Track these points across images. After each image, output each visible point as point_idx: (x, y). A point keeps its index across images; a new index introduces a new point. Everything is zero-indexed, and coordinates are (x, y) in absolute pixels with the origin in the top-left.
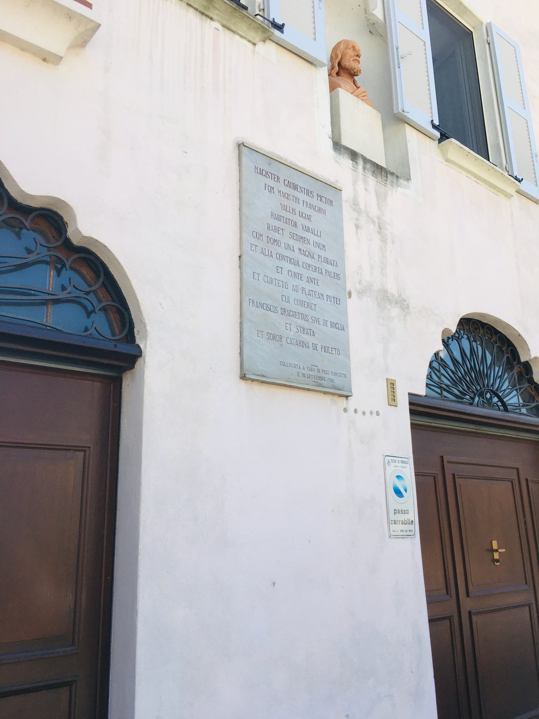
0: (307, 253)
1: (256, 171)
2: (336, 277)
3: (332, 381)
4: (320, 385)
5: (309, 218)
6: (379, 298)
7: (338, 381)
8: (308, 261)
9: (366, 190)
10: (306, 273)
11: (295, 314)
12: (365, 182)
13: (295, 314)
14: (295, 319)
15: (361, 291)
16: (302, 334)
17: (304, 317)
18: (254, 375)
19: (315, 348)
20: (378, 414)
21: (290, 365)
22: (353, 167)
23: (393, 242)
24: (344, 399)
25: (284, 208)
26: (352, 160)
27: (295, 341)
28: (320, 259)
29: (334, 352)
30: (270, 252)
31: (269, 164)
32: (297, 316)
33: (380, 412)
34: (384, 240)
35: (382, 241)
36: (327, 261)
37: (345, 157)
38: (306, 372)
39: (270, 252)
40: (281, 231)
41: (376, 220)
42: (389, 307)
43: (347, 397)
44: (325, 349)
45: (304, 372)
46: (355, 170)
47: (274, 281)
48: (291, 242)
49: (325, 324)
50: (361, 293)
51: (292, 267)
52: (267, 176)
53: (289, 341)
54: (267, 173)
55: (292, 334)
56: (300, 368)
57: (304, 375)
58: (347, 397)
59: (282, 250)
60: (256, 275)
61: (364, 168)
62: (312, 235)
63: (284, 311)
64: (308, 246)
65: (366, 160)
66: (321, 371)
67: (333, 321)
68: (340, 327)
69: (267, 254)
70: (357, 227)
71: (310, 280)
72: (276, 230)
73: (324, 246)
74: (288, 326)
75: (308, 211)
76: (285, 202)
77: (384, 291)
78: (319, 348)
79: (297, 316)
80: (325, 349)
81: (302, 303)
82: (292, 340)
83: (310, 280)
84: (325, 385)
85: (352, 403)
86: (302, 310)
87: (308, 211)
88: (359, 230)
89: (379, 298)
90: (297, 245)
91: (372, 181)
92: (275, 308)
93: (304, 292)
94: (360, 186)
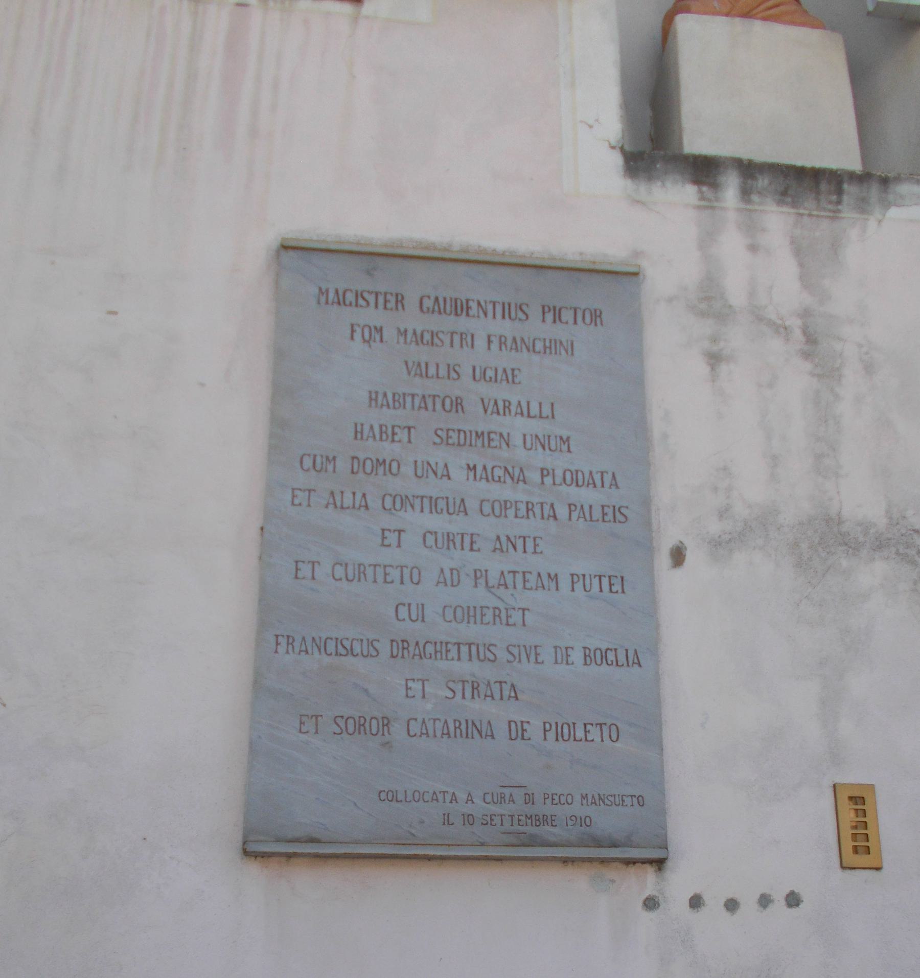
0: (498, 472)
1: (323, 299)
2: (610, 517)
3: (585, 821)
4: (533, 841)
5: (510, 377)
6: (804, 546)
7: (607, 821)
8: (506, 492)
9: (753, 248)
10: (487, 527)
11: (442, 649)
12: (751, 227)
13: (442, 649)
14: (442, 664)
15: (727, 537)
16: (468, 703)
17: (480, 652)
18: (278, 840)
19: (518, 732)
20: (793, 900)
21: (418, 797)
22: (702, 198)
23: (869, 368)
24: (650, 871)
25: (421, 371)
26: (697, 182)
27: (439, 725)
28: (548, 480)
29: (594, 733)
30: (359, 496)
31: (369, 273)
32: (453, 653)
33: (891, 825)
34: (828, 372)
35: (820, 376)
36: (575, 479)
37: (668, 184)
38: (479, 808)
39: (359, 496)
40: (402, 435)
41: (795, 323)
42: (844, 563)
43: (659, 864)
44: (561, 731)
45: (468, 809)
46: (708, 206)
47: (370, 571)
48: (438, 456)
49: (563, 655)
50: (720, 546)
51: (437, 522)
52: (361, 302)
53: (415, 728)
54: (359, 295)
55: (429, 706)
56: (454, 799)
57: (469, 819)
58: (659, 864)
59: (405, 483)
60: (306, 570)
61: (745, 193)
62: (520, 421)
63: (400, 647)
64: (505, 453)
65: (748, 169)
66: (538, 798)
67: (593, 643)
68: (635, 655)
69: (348, 502)
70: (714, 359)
71: (504, 545)
72: (387, 433)
73: (566, 441)
74: (416, 686)
75: (504, 360)
76: (421, 354)
77: (828, 520)
78: (534, 731)
79: (453, 653)
80: (561, 731)
81: (471, 614)
82: (430, 725)
83: (504, 545)
84: (552, 839)
85: (679, 883)
86: (470, 631)
87: (504, 360)
88: (724, 368)
89: (804, 546)
90: (457, 461)
91: (776, 220)
92: (371, 643)
93: (482, 581)
94: (731, 244)
